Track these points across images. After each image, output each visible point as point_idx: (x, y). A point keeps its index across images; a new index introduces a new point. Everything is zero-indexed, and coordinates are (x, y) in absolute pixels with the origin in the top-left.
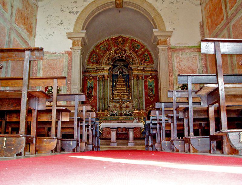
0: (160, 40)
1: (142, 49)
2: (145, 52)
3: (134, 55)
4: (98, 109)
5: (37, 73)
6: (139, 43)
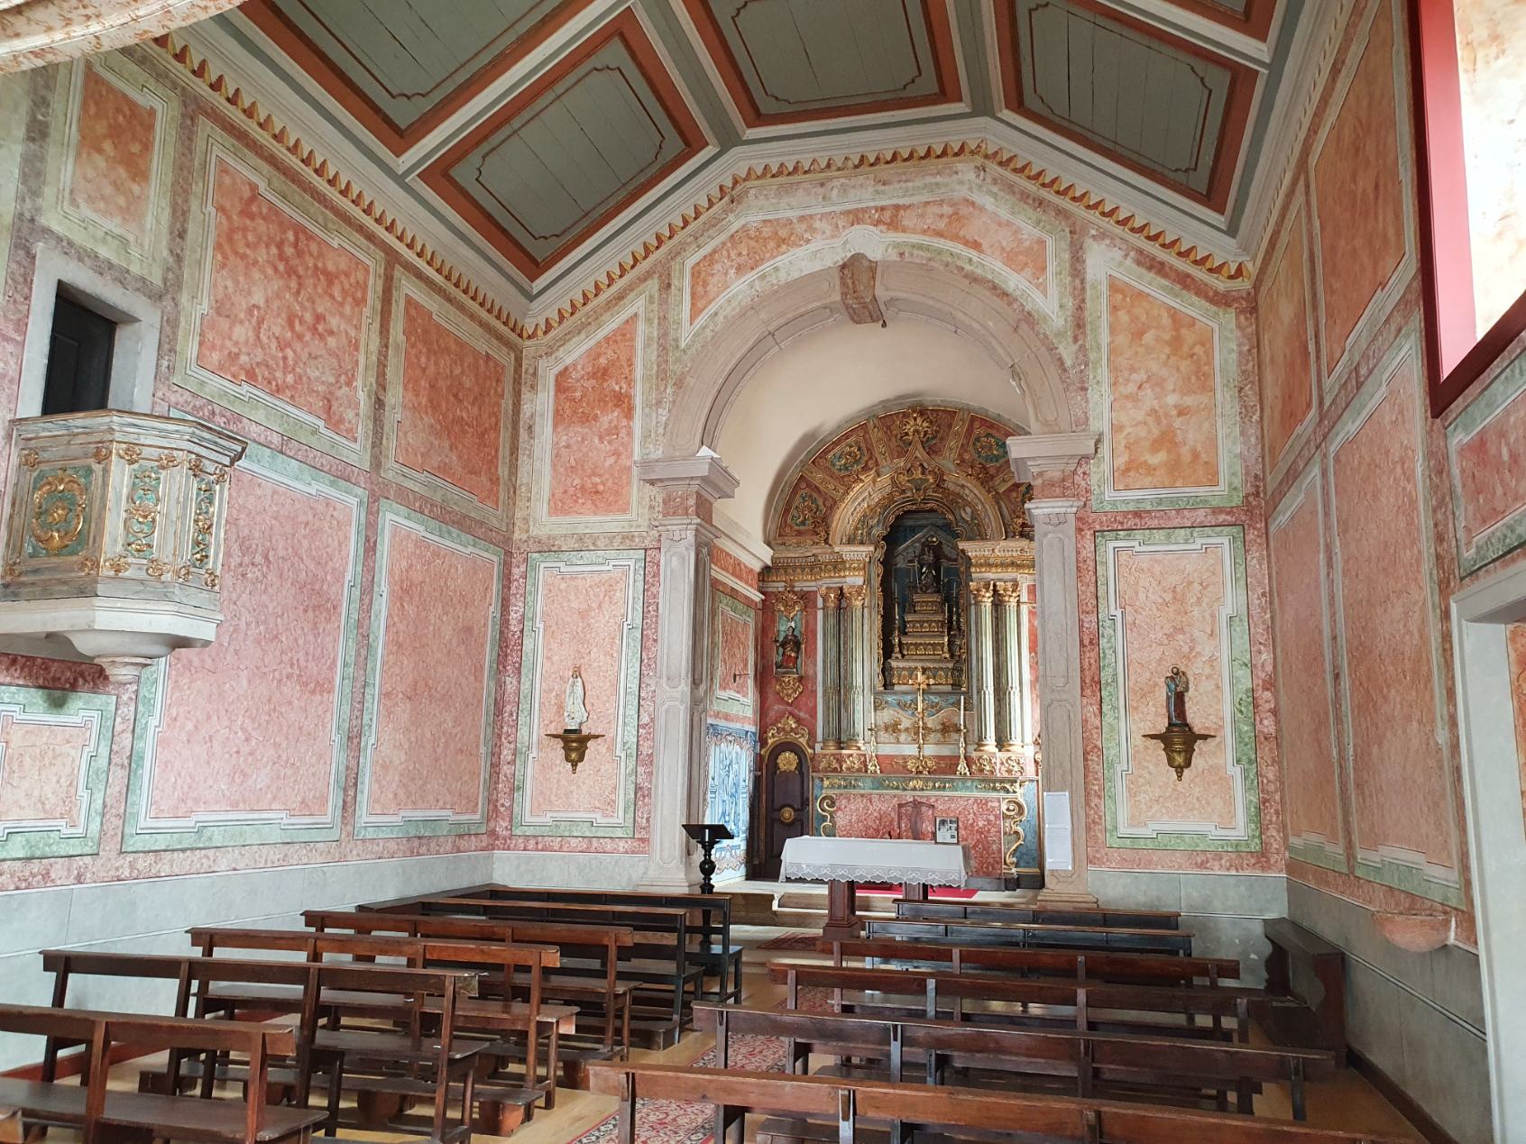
0: (1041, 474)
3: (973, 491)
4: (820, 737)
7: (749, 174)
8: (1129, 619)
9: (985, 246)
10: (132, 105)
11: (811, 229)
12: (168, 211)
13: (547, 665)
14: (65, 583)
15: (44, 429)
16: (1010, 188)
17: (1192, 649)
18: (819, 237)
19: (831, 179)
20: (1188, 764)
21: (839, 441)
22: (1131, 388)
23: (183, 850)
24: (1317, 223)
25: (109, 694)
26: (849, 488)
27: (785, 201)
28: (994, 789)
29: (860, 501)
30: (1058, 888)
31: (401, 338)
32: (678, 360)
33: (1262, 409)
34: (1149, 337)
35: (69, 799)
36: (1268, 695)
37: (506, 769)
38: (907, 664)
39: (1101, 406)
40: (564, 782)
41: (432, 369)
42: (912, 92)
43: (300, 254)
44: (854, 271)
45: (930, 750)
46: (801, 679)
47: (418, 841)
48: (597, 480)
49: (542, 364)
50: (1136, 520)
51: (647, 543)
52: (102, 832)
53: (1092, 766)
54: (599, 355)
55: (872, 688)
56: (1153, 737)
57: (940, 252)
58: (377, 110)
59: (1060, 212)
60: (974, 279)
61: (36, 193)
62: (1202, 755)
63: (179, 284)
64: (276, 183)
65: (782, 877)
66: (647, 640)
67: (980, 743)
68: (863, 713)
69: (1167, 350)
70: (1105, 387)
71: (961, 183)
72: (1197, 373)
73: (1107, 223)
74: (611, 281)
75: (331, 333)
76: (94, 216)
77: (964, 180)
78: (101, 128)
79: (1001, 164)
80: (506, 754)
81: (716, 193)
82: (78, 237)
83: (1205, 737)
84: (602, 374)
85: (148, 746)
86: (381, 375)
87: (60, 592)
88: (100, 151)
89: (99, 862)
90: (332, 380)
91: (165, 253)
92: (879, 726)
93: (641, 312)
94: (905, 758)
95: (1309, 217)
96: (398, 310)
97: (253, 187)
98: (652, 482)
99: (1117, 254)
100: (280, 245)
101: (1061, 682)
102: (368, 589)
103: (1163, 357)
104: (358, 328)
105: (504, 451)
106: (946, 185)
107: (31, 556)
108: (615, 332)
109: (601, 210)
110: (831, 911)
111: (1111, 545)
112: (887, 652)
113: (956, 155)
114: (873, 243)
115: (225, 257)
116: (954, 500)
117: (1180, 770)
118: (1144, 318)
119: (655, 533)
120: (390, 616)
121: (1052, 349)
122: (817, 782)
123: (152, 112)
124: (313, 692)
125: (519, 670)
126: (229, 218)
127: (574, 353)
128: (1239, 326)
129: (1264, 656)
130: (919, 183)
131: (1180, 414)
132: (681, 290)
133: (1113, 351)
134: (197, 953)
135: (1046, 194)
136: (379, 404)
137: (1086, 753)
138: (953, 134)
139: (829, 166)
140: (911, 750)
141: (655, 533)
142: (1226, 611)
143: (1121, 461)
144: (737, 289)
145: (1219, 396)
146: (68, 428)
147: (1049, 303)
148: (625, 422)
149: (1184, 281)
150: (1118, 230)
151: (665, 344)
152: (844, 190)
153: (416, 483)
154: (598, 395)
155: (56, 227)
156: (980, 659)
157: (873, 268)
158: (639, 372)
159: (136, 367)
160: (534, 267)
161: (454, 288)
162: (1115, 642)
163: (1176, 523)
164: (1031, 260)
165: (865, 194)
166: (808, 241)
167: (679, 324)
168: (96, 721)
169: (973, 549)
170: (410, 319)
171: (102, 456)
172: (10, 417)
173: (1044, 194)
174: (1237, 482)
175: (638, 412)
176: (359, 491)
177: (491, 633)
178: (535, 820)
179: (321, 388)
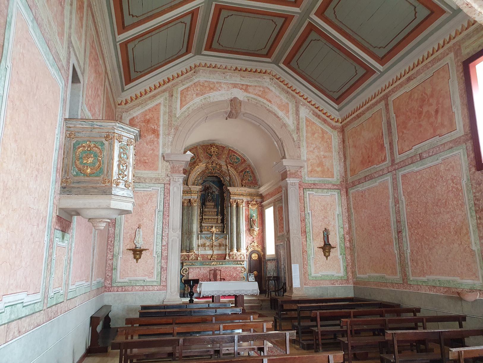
0: (289, 170)
1: (242, 163)
3: (232, 171)
6: (239, 156)
8: (313, 214)
11: (220, 86)
13: (126, 224)
14: (96, 188)
16: (279, 86)
17: (329, 223)
22: (312, 149)
28: (238, 264)
32: (176, 121)
34: (316, 135)
36: (347, 236)
37: (110, 262)
44: (234, 102)
45: (216, 252)
48: (146, 158)
49: (124, 115)
50: (313, 186)
51: (165, 182)
53: (305, 256)
54: (146, 115)
56: (320, 248)
57: (260, 101)
59: (293, 96)
66: (166, 214)
67: (231, 249)
72: (328, 147)
73: (305, 102)
77: (266, 81)
81: (189, 69)
84: (148, 121)
87: (93, 192)
94: (207, 255)
107: (74, 176)
111: (308, 192)
114: (241, 95)
118: (315, 130)
127: (137, 112)
131: (324, 158)
132: (177, 98)
135: (289, 90)
137: (303, 252)
139: (226, 68)
140: (210, 252)
141: (168, 178)
142: (337, 212)
143: (310, 169)
144: (198, 101)
147: (290, 121)
148: (156, 139)
149: (325, 121)
151: (171, 114)
156: (232, 224)
157: (240, 102)
158: (161, 123)
162: (309, 220)
163: (324, 187)
165: (237, 79)
166: (220, 90)
167: (176, 109)
169: (231, 189)
173: (289, 90)
174: (338, 178)
175: (161, 137)
178: (122, 280)
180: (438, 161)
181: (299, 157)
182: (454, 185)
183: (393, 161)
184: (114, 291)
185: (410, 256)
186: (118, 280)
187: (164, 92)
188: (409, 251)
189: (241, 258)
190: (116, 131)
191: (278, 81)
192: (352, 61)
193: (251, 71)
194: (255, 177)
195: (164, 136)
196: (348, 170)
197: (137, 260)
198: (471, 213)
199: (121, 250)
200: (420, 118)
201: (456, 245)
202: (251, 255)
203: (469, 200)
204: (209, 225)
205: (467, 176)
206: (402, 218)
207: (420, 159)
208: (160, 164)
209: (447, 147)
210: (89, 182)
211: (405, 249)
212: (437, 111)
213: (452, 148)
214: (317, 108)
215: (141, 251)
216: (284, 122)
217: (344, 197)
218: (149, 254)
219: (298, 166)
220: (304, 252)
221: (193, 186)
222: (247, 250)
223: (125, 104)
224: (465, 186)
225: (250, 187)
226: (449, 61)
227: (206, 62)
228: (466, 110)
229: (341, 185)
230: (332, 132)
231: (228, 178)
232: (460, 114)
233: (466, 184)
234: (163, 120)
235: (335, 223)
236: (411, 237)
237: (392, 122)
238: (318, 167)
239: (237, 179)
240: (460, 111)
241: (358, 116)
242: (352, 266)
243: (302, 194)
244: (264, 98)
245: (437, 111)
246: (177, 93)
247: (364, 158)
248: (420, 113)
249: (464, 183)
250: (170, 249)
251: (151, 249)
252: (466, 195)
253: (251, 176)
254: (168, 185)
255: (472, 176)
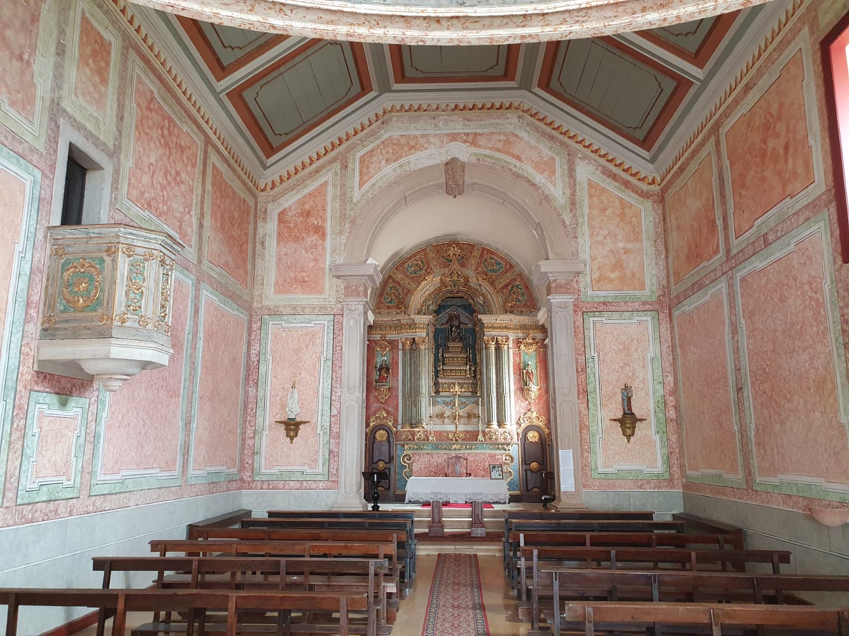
0: (555, 281)
1: (507, 271)
2: (516, 280)
3: (486, 287)
4: (400, 421)
5: (258, 361)
6: (501, 258)
7: (392, 108)
8: (602, 358)
9: (523, 158)
10: (101, 37)
11: (428, 142)
12: (116, 104)
13: (275, 380)
14: (89, 329)
15: (70, 233)
16: (536, 129)
17: (633, 374)
18: (432, 146)
19: (439, 116)
20: (633, 434)
21: (411, 257)
22: (600, 238)
23: (116, 494)
24: (727, 162)
25: (86, 398)
26: (419, 283)
27: (413, 125)
28: (498, 449)
29: (424, 291)
30: (567, 501)
31: (210, 187)
32: (352, 209)
33: (667, 252)
34: (608, 212)
35: (67, 464)
36: (672, 398)
37: (249, 442)
38: (447, 381)
39: (585, 244)
40: (285, 449)
41: (222, 206)
42: (491, 73)
43: (170, 134)
44: (452, 167)
45: (461, 428)
46: (389, 389)
47: (213, 485)
48: (304, 274)
49: (270, 206)
50: (604, 307)
51: (335, 311)
52: (82, 484)
53: (584, 436)
54: (305, 203)
55: (429, 393)
56: (615, 420)
57: (499, 160)
58: (214, 53)
59: (562, 144)
60: (518, 176)
61: (60, 88)
62: (640, 429)
63: (120, 148)
64: (161, 92)
65: (407, 500)
66: (336, 365)
67: (489, 424)
68: (426, 408)
69: (618, 219)
70: (587, 237)
71: (510, 124)
72: (633, 232)
73: (587, 152)
74: (312, 162)
75: (182, 182)
76: (85, 104)
77: (511, 123)
78: (88, 51)
79: (531, 115)
80: (249, 433)
81: (373, 118)
82: (78, 117)
83: (641, 420)
84: (308, 214)
85: (102, 429)
86: (202, 209)
87: (86, 335)
88: (88, 65)
89: (80, 502)
90: (182, 210)
91: (115, 129)
92: (434, 416)
93: (330, 180)
94: (447, 432)
95: (719, 157)
96: (209, 170)
97: (152, 93)
98: (338, 277)
99: (592, 168)
100: (162, 129)
101: (567, 391)
102: (195, 335)
103: (616, 223)
104: (193, 180)
105: (250, 256)
106: (502, 124)
107: (62, 312)
108: (315, 190)
109: (312, 121)
110: (433, 518)
111: (592, 319)
112: (437, 376)
113: (507, 109)
114: (463, 152)
115: (139, 134)
116: (474, 293)
117: (629, 438)
118: (606, 201)
119: (339, 306)
120: (204, 351)
121: (559, 215)
122: (399, 446)
123: (110, 44)
124: (171, 397)
125: (257, 383)
126: (141, 110)
127: (290, 201)
128: (654, 209)
129: (669, 378)
130: (487, 122)
131: (625, 253)
132: (353, 170)
133: (591, 218)
134: (157, 555)
135: (556, 134)
136: (201, 226)
137: (581, 429)
138: (505, 97)
139: (437, 108)
140: (451, 428)
141: (339, 306)
142: (651, 354)
143: (596, 275)
144: (388, 171)
145: (645, 245)
146: (87, 233)
147: (557, 191)
148: (320, 242)
149: (626, 184)
150: (593, 155)
151: (344, 198)
152: (446, 122)
153: (215, 272)
154: (304, 226)
155: (68, 110)
156: (489, 379)
157: (463, 165)
158: (329, 214)
159: (102, 197)
160: (270, 150)
161: (232, 161)
162: (594, 368)
163: (624, 308)
164: (547, 167)
165: (458, 125)
166: (426, 148)
167: (352, 188)
168: (80, 414)
169: (485, 319)
170: (214, 177)
171: (111, 251)
172: (46, 225)
173: (554, 133)
174: (654, 289)
175: (328, 237)
176: (192, 277)
177: (243, 361)
178: (268, 471)
179: (178, 215)
180: (789, 248)
181: (575, 255)
182: (813, 294)
183: (728, 251)
184: (256, 488)
185: (756, 436)
186: (263, 471)
187: (332, 162)
188: (753, 427)
189: (505, 439)
190: (122, 240)
191: (535, 121)
192: (647, 68)
193: (482, 108)
194: (531, 295)
195: (334, 236)
196: (671, 272)
197: (292, 438)
198: (837, 348)
199: (267, 423)
200: (763, 163)
201: (818, 414)
202: (526, 434)
203: (834, 323)
204: (451, 381)
205: (831, 275)
206: (743, 363)
207: (765, 246)
208: (327, 282)
209: (802, 218)
210: (81, 320)
211: (748, 422)
212: (786, 148)
213: (808, 219)
214: (611, 161)
215: (297, 425)
216: (546, 193)
217: (665, 326)
218: (310, 430)
219: (571, 273)
220: (583, 427)
221: (418, 316)
222: (519, 424)
223: (272, 188)
224: (828, 296)
225: (521, 313)
226: (802, 45)
227: (402, 102)
228: (828, 140)
229: (659, 301)
230: (642, 203)
231: (480, 300)
232: (820, 150)
233: (830, 291)
234: (331, 207)
235: (646, 373)
236: (755, 399)
237: (725, 176)
238: (613, 271)
239: (496, 300)
240: (819, 144)
241: (682, 170)
242: (677, 456)
243: (579, 323)
244: (508, 153)
245: (786, 148)
246: (354, 162)
247: (690, 249)
248: (764, 154)
249: (826, 288)
250: (343, 422)
251: (313, 422)
252: (830, 312)
253: (523, 295)
254: (340, 317)
255: (838, 274)
